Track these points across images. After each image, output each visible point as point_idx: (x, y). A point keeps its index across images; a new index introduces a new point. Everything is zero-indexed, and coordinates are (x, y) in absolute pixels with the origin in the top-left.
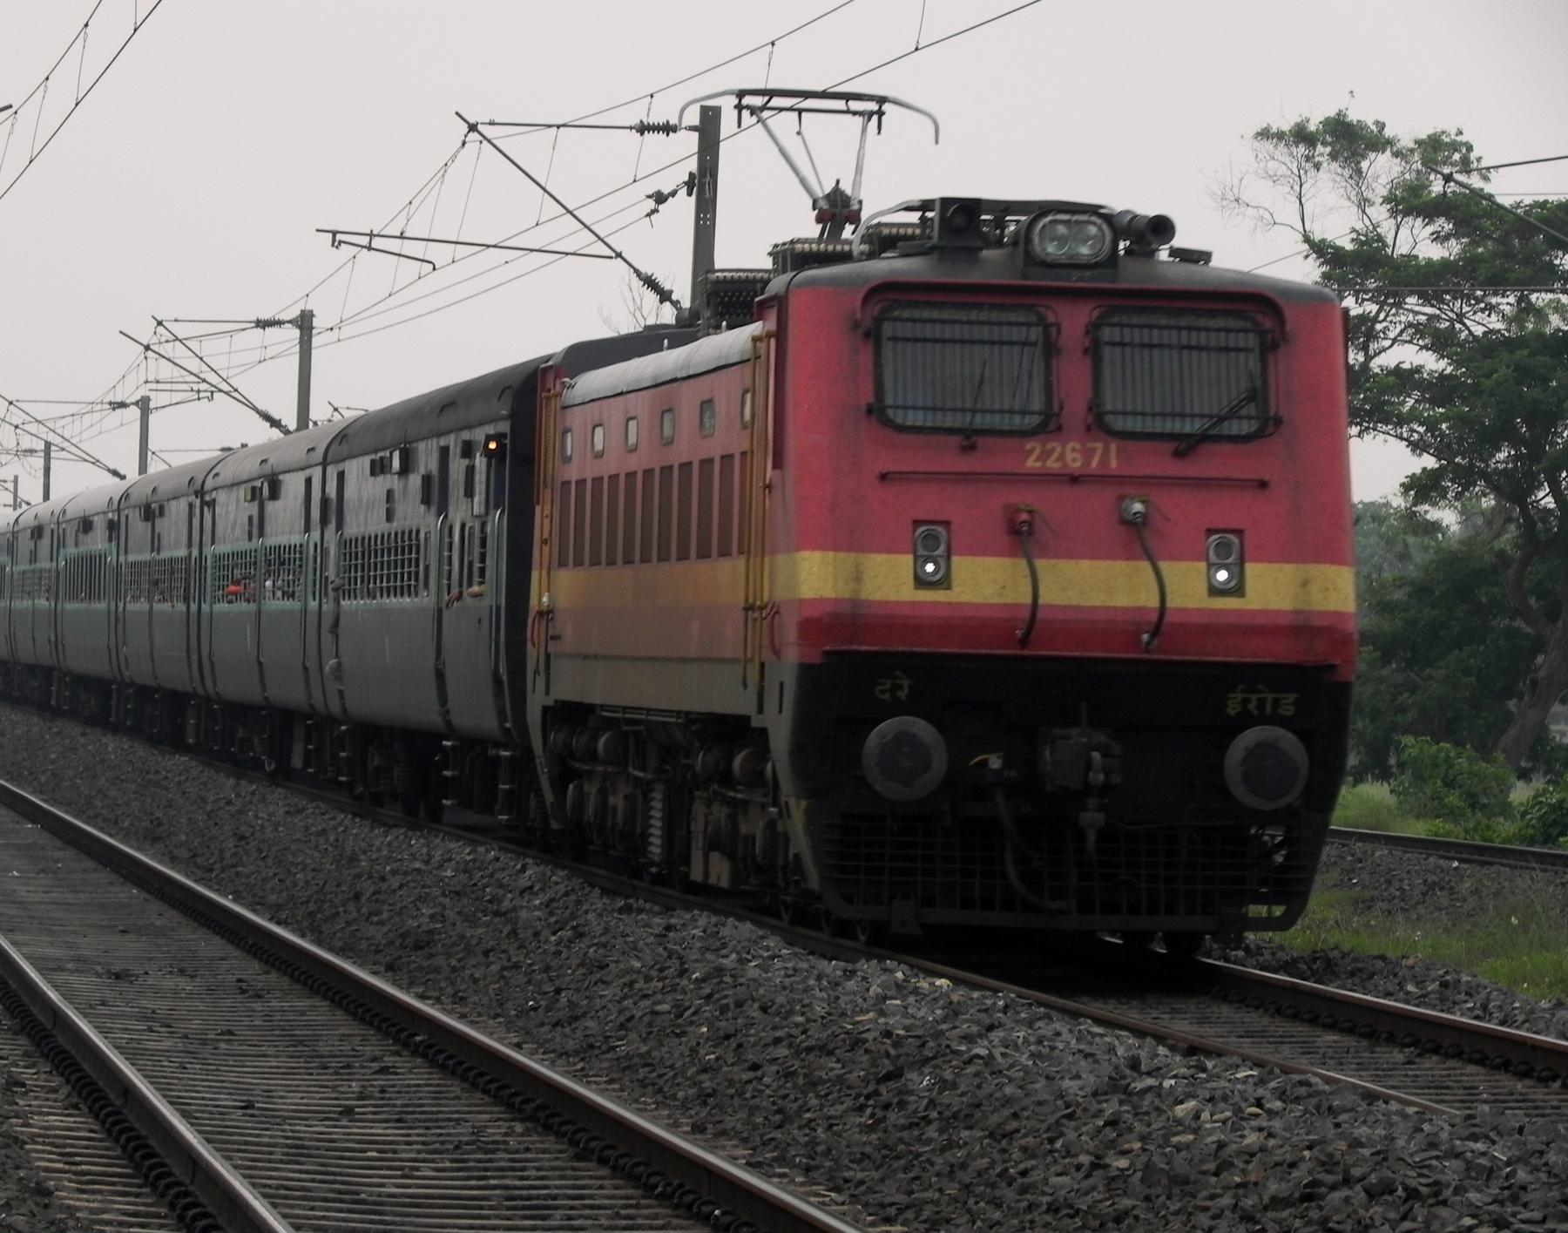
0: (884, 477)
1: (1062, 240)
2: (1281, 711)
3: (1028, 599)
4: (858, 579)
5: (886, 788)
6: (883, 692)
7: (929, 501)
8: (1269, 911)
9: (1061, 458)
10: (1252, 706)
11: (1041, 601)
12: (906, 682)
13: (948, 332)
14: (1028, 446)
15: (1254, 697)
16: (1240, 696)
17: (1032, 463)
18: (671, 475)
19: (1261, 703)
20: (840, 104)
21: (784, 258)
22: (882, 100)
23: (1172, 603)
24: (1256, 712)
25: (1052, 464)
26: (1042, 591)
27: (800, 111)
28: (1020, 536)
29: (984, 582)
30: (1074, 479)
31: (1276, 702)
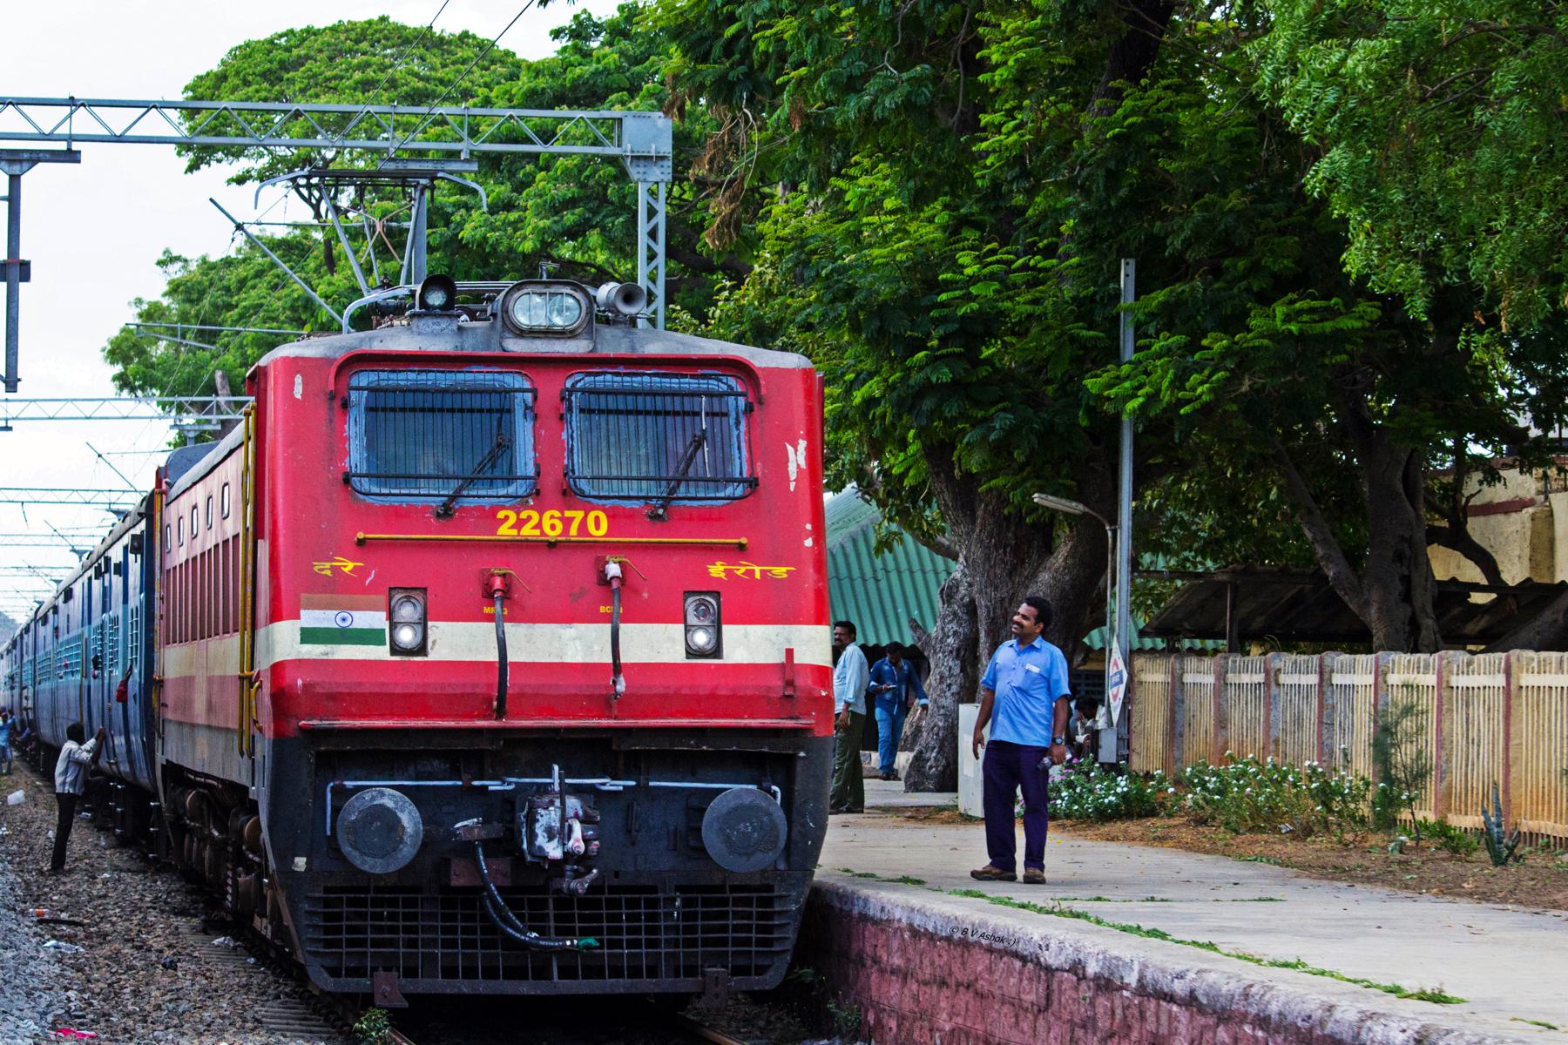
9: (539, 526)
17: (505, 531)
25: (528, 531)
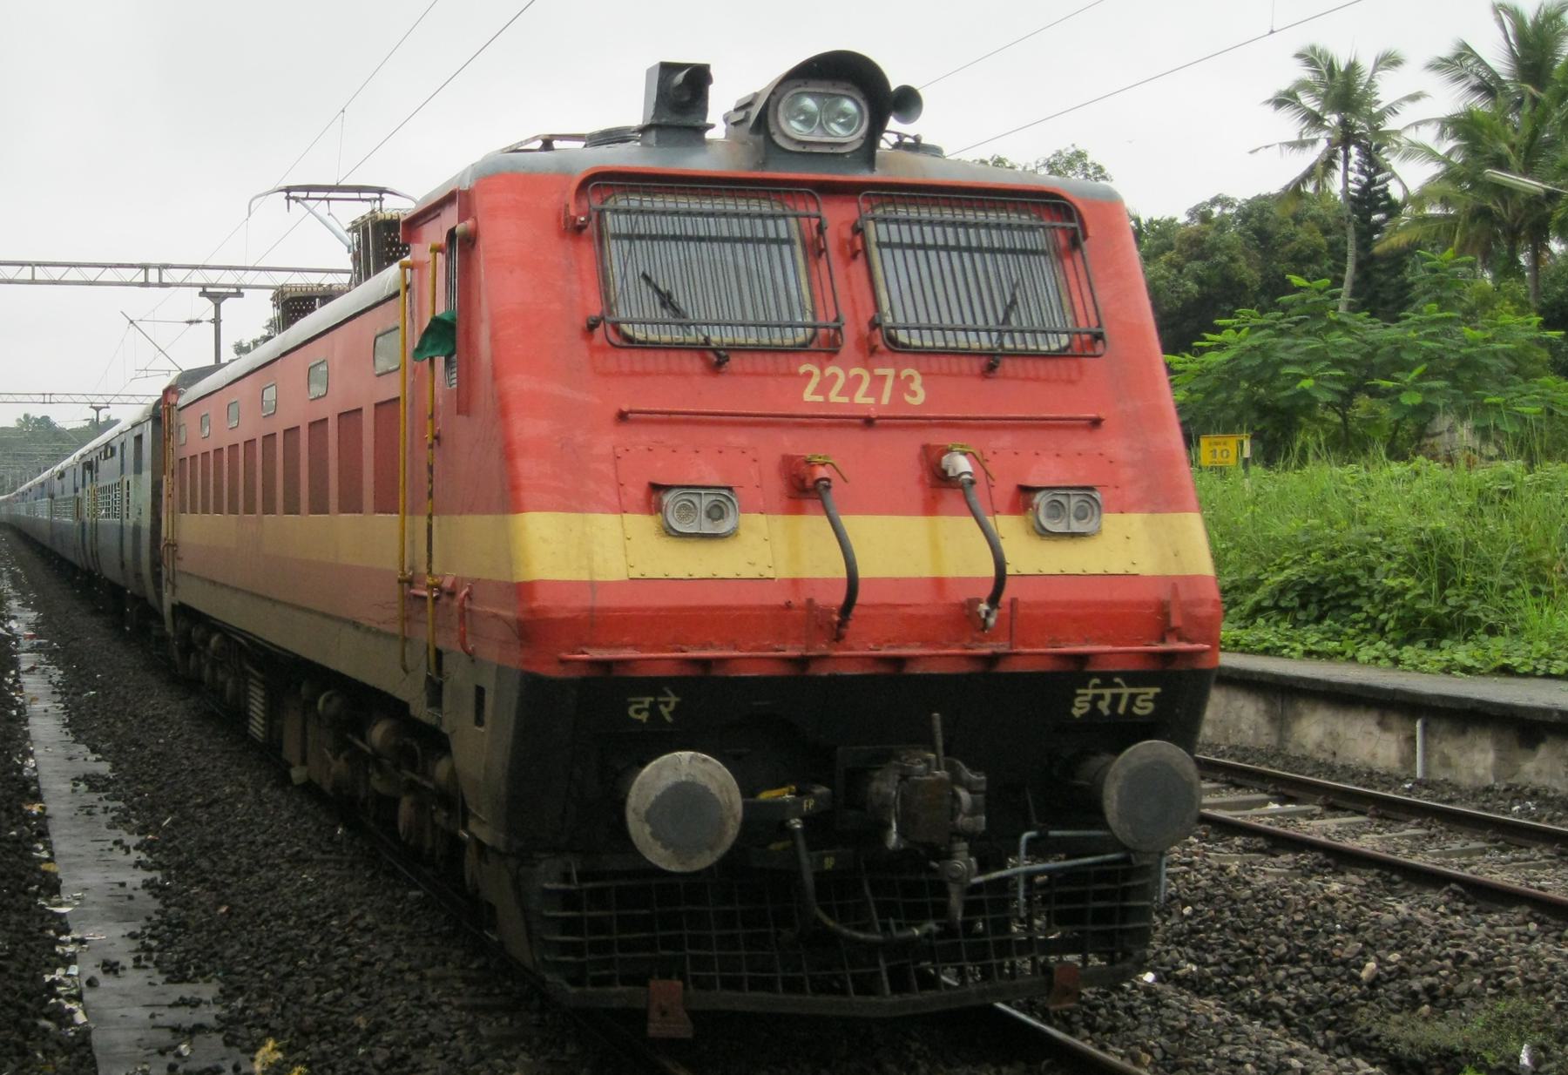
0: (622, 417)
1: (809, 121)
2: (1136, 710)
3: (989, 571)
4: (935, 546)
5: (658, 855)
6: (638, 711)
7: (660, 456)
8: (1085, 961)
10: (1103, 706)
11: (1010, 570)
12: (674, 700)
13: (702, 227)
14: (803, 369)
15: (1107, 692)
16: (1091, 692)
18: (254, 447)
19: (1116, 699)
20: (356, 195)
21: (366, 231)
22: (381, 191)
23: (863, 573)
24: (1106, 712)
26: (1008, 558)
27: (328, 200)
28: (803, 490)
29: (773, 551)
30: (868, 422)
31: (1133, 697)
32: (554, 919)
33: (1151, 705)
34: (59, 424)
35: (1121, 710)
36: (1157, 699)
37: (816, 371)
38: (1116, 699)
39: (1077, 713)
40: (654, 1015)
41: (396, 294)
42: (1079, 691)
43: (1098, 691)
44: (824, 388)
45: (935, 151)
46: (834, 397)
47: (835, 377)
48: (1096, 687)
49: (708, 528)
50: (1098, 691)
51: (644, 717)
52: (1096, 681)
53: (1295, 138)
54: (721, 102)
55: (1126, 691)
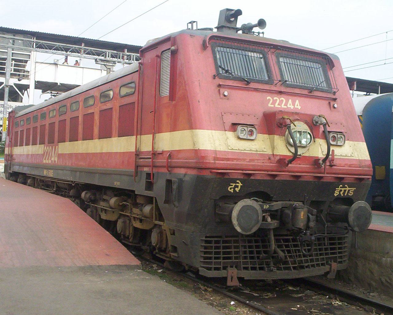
2: (349, 194)
15: (343, 189)
16: (339, 189)
19: (345, 191)
32: (202, 251)
33: (352, 193)
34: (291, 43)
35: (346, 195)
36: (354, 192)
37: (271, 98)
38: (345, 191)
39: (335, 195)
40: (229, 279)
41: (137, 71)
42: (337, 189)
43: (341, 189)
44: (274, 103)
45: (33, 105)
46: (276, 105)
47: (276, 100)
48: (341, 187)
49: (249, 138)
50: (341, 189)
51: (232, 191)
52: (341, 186)
53: (14, 166)
54: (241, 22)
55: (348, 189)
